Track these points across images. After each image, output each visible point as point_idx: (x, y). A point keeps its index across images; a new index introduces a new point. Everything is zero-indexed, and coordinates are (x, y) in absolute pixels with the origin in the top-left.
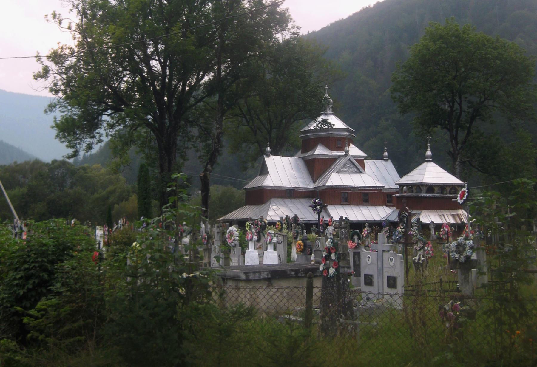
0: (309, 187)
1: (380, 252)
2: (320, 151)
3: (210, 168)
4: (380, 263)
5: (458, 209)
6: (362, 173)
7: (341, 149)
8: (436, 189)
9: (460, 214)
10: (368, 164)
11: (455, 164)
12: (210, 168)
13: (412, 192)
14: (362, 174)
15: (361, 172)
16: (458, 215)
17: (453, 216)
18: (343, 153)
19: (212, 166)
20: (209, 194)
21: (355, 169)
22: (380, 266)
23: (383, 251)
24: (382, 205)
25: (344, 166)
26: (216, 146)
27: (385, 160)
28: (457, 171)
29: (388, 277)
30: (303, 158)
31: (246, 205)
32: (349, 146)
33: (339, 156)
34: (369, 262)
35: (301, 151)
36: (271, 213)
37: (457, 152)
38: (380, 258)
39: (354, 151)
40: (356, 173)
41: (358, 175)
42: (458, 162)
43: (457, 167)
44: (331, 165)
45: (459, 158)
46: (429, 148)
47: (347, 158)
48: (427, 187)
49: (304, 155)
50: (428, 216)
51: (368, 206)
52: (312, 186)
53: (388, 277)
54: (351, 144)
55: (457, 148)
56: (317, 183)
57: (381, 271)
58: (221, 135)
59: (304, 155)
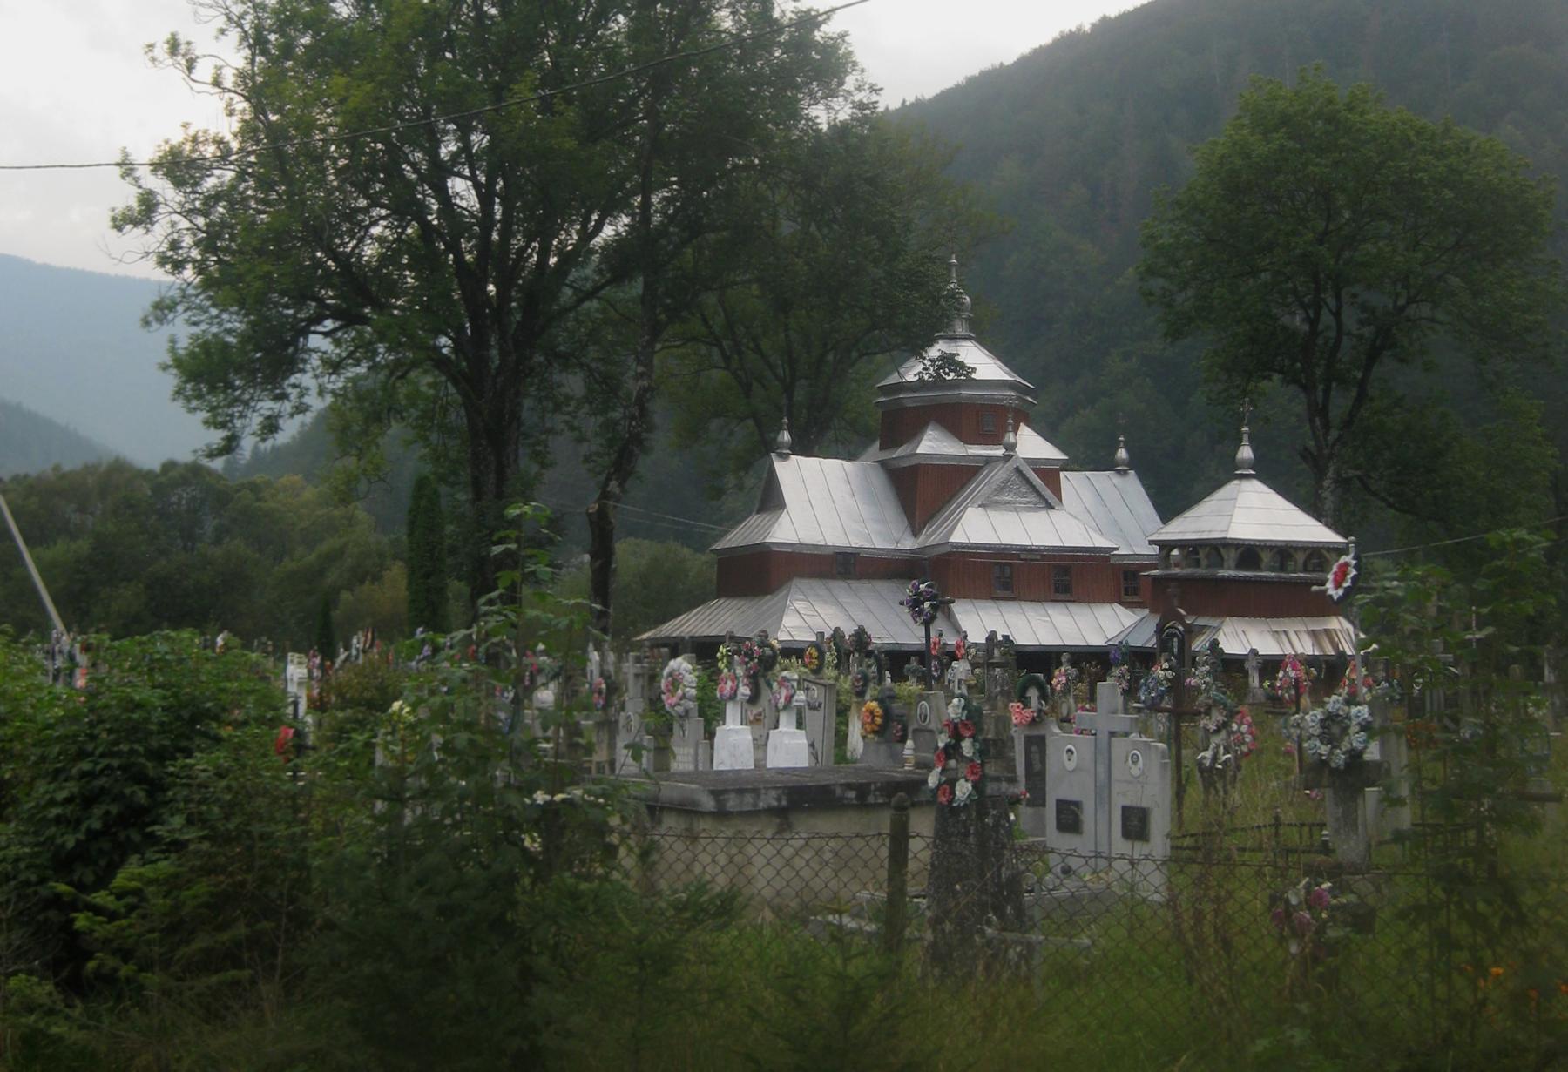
0: (900, 547)
1: (1104, 737)
2: (934, 444)
3: (617, 490)
4: (1101, 769)
5: (1329, 615)
6: (1053, 508)
7: (994, 439)
8: (1266, 557)
9: (1334, 630)
10: (1071, 482)
11: (1321, 487)
12: (617, 490)
13: (1197, 564)
14: (1052, 513)
15: (1050, 507)
16: (1327, 632)
17: (1314, 634)
18: (999, 451)
19: (621, 485)
20: (613, 566)
21: (1033, 498)
22: (1102, 776)
23: (1112, 734)
24: (1111, 602)
25: (1001, 489)
26: (634, 427)
27: (1119, 472)
28: (1326, 507)
29: (1125, 809)
30: (883, 464)
31: (718, 597)
32: (1016, 431)
33: (989, 460)
34: (1071, 766)
35: (877, 445)
36: (1239, 516)
37: (1326, 452)
38: (1103, 756)
39: (1031, 445)
40: (1036, 509)
41: (1043, 514)
42: (1330, 481)
43: (1326, 494)
44: (963, 486)
45: (1331, 469)
46: (1246, 437)
47: (1011, 465)
48: (1239, 551)
49: (886, 455)
50: (1241, 635)
51: (1069, 604)
52: (908, 543)
53: (1125, 809)
54: (1022, 426)
55: (1326, 440)
56: (922, 537)
57: (1104, 791)
58: (648, 396)
59: (886, 455)
